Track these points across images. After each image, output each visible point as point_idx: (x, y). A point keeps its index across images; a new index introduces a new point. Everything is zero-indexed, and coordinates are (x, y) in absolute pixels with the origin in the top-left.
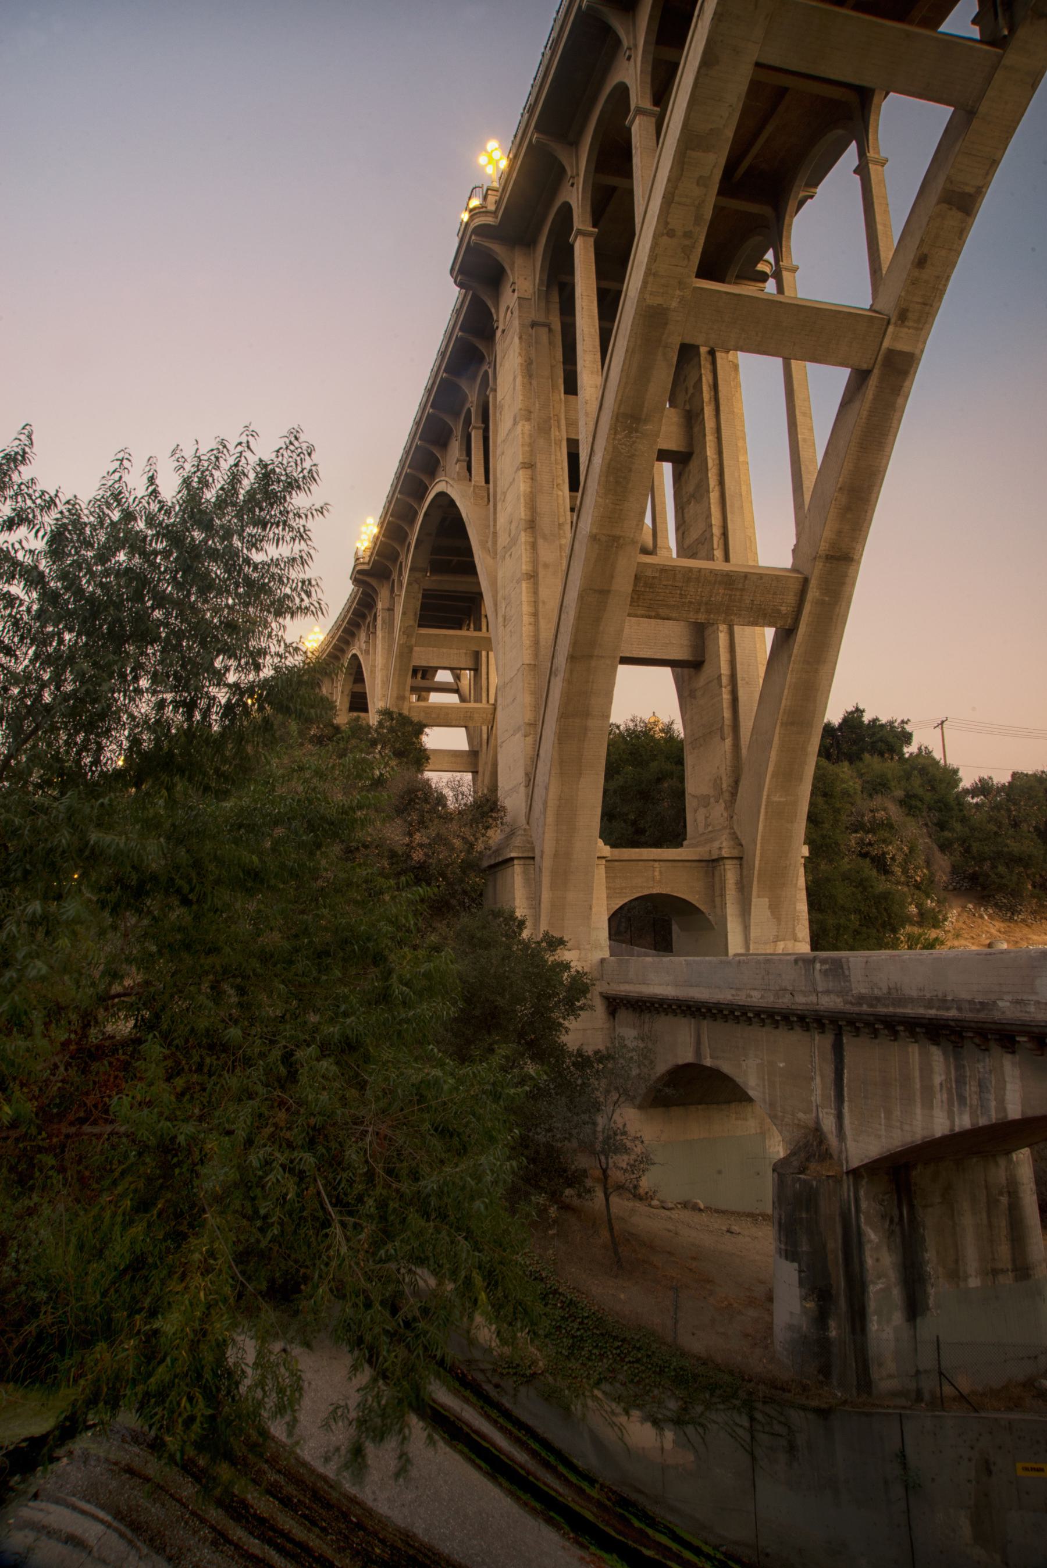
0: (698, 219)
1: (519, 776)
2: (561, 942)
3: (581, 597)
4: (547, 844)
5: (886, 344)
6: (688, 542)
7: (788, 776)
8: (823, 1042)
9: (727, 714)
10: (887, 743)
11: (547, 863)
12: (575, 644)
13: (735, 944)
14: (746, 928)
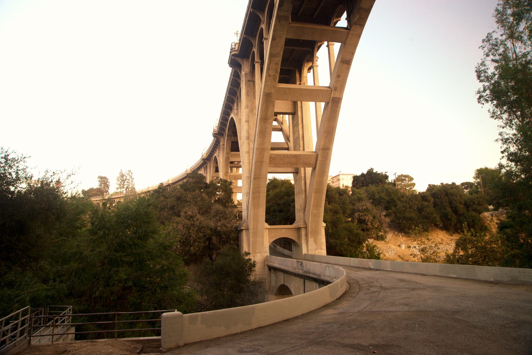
0: (276, 72)
1: (246, 206)
2: (249, 254)
3: (255, 163)
4: (251, 227)
5: (332, 96)
6: (295, 138)
7: (317, 206)
8: (302, 280)
9: (303, 188)
10: (380, 179)
11: (251, 231)
12: (255, 175)
13: (304, 251)
14: (307, 246)
